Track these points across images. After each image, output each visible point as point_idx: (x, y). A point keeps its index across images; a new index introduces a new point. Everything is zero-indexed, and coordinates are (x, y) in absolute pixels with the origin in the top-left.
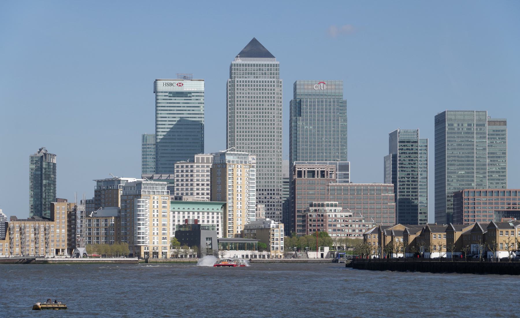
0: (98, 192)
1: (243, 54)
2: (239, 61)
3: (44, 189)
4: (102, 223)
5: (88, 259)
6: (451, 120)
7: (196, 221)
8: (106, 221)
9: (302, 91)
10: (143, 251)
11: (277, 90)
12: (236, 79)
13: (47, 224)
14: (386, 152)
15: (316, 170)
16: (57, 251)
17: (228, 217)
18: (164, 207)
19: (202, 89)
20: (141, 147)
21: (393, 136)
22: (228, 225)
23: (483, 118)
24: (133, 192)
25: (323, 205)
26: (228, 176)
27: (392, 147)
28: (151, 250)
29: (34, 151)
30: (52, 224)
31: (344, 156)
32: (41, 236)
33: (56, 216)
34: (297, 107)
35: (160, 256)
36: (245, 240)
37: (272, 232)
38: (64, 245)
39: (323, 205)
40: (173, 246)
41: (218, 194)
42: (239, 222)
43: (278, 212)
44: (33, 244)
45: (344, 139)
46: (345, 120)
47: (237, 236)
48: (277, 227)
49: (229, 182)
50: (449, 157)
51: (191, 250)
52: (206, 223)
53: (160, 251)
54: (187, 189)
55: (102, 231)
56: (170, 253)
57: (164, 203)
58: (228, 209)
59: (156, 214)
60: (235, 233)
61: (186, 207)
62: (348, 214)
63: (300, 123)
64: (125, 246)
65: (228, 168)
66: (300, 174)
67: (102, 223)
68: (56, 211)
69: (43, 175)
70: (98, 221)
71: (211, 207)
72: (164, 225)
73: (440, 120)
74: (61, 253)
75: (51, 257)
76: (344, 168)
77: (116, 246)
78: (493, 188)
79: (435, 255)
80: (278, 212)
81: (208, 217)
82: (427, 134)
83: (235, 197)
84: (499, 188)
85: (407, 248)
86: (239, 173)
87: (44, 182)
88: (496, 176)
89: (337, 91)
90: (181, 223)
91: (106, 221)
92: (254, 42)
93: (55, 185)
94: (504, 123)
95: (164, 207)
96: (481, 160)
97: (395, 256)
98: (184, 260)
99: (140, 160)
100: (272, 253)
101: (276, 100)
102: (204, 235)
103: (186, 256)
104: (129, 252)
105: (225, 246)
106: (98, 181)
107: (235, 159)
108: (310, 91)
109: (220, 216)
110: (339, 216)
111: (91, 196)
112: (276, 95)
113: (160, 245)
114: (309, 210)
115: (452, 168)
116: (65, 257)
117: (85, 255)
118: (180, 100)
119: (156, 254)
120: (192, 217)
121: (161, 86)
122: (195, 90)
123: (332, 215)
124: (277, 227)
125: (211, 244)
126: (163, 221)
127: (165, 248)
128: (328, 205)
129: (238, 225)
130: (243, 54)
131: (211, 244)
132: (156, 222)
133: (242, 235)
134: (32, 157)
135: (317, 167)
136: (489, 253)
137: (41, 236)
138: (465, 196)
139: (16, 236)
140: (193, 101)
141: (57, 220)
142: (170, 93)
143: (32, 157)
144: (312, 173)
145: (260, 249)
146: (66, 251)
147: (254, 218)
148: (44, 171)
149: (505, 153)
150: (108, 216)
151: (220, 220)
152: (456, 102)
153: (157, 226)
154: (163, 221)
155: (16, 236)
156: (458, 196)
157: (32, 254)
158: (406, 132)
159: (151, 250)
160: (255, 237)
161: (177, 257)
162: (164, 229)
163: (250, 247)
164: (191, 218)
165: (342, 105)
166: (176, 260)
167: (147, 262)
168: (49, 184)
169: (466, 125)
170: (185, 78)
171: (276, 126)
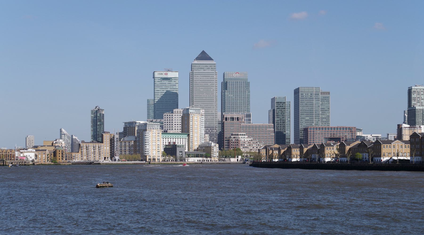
0: (124, 128)
1: (198, 59)
2: (196, 62)
3: (98, 127)
5: (120, 162)
6: (302, 91)
7: (174, 143)
8: (129, 143)
9: (227, 77)
10: (148, 158)
11: (215, 76)
12: (194, 71)
13: (100, 144)
14: (270, 108)
16: (105, 158)
17: (190, 141)
18: (158, 136)
19: (177, 76)
21: (273, 100)
25: (238, 135)
26: (190, 120)
27: (273, 105)
28: (152, 158)
29: (93, 108)
30: (102, 144)
32: (97, 150)
33: (104, 140)
34: (225, 86)
35: (156, 160)
36: (199, 153)
38: (108, 155)
39: (238, 135)
40: (163, 155)
41: (185, 129)
42: (196, 143)
43: (215, 138)
46: (249, 92)
47: (195, 150)
48: (215, 146)
49: (191, 123)
50: (301, 110)
51: (172, 158)
52: (179, 144)
53: (156, 158)
54: (170, 127)
55: (127, 148)
56: (161, 159)
57: (158, 134)
59: (154, 139)
60: (194, 149)
61: (169, 136)
63: (226, 93)
64: (139, 156)
65: (191, 116)
68: (104, 138)
69: (97, 120)
70: (125, 143)
73: (297, 92)
74: (107, 159)
75: (102, 161)
76: (249, 116)
77: (134, 156)
79: (294, 160)
80: (215, 138)
81: (180, 141)
82: (290, 99)
83: (194, 131)
84: (326, 126)
85: (280, 156)
86: (196, 119)
87: (98, 123)
88: (324, 120)
89: (245, 77)
90: (167, 144)
91: (129, 143)
92: (203, 52)
95: (158, 136)
97: (274, 160)
98: (168, 162)
100: (213, 159)
101: (214, 82)
102: (178, 150)
103: (169, 160)
106: (125, 123)
108: (231, 77)
109: (186, 140)
110: (246, 140)
111: (122, 130)
112: (214, 79)
113: (156, 155)
114: (231, 137)
115: (302, 116)
116: (109, 161)
117: (119, 160)
119: (154, 159)
120: (172, 141)
121: (156, 75)
123: (243, 139)
124: (215, 146)
125: (182, 154)
127: (159, 156)
128: (240, 135)
129: (196, 145)
130: (198, 59)
131: (182, 154)
132: (154, 144)
133: (197, 150)
134: (92, 111)
135: (235, 116)
137: (97, 150)
138: (309, 130)
139: (84, 151)
140: (173, 82)
142: (161, 78)
143: (92, 111)
144: (233, 119)
145: (206, 157)
146: (109, 158)
149: (329, 109)
150: (130, 140)
151: (186, 142)
152: (304, 84)
153: (155, 146)
155: (84, 151)
156: (306, 130)
157: (92, 160)
159: (152, 158)
160: (204, 151)
161: (165, 161)
162: (158, 147)
163: (202, 156)
164: (172, 141)
165: (247, 84)
166: (164, 162)
167: (150, 163)
168: (101, 124)
169: (309, 94)
170: (169, 71)
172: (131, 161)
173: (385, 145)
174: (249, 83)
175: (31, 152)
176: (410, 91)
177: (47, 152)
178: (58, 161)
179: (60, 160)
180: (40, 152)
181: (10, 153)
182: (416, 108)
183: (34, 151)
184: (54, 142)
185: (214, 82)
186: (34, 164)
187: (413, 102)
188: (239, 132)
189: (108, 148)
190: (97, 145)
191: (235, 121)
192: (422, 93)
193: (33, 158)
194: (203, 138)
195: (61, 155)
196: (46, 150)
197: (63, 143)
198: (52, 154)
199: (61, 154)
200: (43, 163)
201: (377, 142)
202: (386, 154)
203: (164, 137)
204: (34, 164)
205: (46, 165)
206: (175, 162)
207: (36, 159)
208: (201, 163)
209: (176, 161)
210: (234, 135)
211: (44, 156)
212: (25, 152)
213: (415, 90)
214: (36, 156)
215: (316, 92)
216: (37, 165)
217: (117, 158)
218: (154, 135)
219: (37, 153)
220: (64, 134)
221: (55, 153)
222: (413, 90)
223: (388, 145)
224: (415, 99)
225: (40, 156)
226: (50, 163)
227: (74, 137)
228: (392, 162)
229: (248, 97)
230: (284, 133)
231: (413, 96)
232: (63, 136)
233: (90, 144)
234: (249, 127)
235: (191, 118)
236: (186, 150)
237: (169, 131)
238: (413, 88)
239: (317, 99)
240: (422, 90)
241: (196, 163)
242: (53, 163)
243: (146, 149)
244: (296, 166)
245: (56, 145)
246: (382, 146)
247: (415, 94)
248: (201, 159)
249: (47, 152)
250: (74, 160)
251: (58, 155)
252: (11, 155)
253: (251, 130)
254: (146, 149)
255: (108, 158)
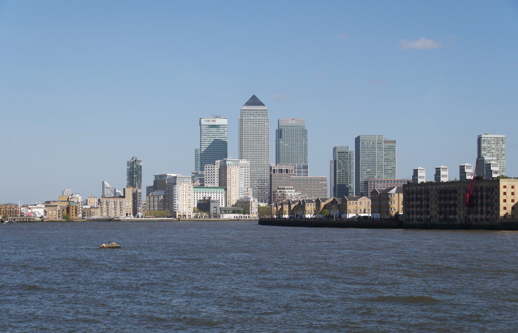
0: (155, 182)
1: (247, 104)
2: (246, 108)
3: (134, 180)
4: (156, 199)
5: (143, 219)
6: (363, 140)
7: (210, 198)
8: (158, 198)
9: (282, 124)
10: (177, 214)
11: (266, 124)
13: (121, 199)
14: (332, 159)
15: (283, 169)
16: (127, 214)
17: (228, 195)
18: (189, 190)
19: (226, 123)
20: (194, 156)
21: (335, 149)
22: (228, 200)
23: (381, 139)
24: (173, 182)
25: (284, 189)
26: (228, 173)
27: (334, 156)
28: (182, 214)
29: (129, 159)
30: (124, 200)
31: (306, 162)
32: (118, 206)
33: (126, 195)
34: (279, 133)
35: (187, 217)
36: (236, 208)
37: (251, 204)
38: (131, 211)
39: (284, 189)
40: (194, 211)
41: (223, 184)
42: (234, 198)
43: (267, 193)
44: (113, 211)
45: (306, 151)
46: (306, 141)
47: (233, 206)
48: (254, 201)
49: (228, 176)
50: (362, 161)
51: (205, 214)
52: (215, 199)
53: (187, 214)
54: (211, 180)
55: (156, 203)
56: (193, 215)
57: (189, 187)
58: (228, 191)
59: (185, 194)
60: (232, 204)
61: (207, 190)
62: (298, 194)
63: (281, 142)
64: (167, 212)
65: (228, 168)
66: (274, 170)
67: (156, 199)
68: (126, 192)
69: (134, 173)
70: (154, 198)
71: (218, 190)
72: (189, 200)
73: (357, 140)
74: (129, 215)
75: (123, 217)
76: (306, 167)
77: (162, 212)
78: (388, 178)
79: (308, 216)
80: (267, 193)
81: (216, 196)
82: (352, 148)
83: (232, 184)
84: (392, 178)
85: (291, 212)
86: (234, 171)
87: (135, 176)
88: (390, 172)
89: (302, 124)
90: (201, 199)
91: (158, 198)
92: (254, 97)
93: (141, 177)
94: (395, 142)
95: (189, 190)
96: (380, 163)
97: (284, 216)
98: (201, 219)
99: (194, 163)
100: (251, 215)
101: (265, 129)
102: (212, 205)
103: (202, 217)
104: (169, 215)
105: (226, 211)
106: (156, 176)
107: (232, 163)
108: (287, 124)
109: (223, 195)
110: (293, 195)
111: (152, 184)
112: (265, 127)
113: (187, 211)
114: (276, 192)
115: (363, 167)
116: (131, 217)
118: (214, 130)
119: (185, 216)
120: (207, 195)
121: (203, 122)
122: (222, 124)
123: (289, 194)
124: (254, 201)
125: (216, 210)
126: (189, 197)
127: (190, 213)
128: (287, 189)
129: (234, 199)
130: (247, 104)
131: (216, 210)
132: (185, 199)
133: (235, 205)
134: (128, 162)
135: (284, 168)
136: (342, 215)
137: (118, 206)
139: (105, 206)
140: (221, 130)
141: (126, 197)
143: (128, 162)
144: (281, 171)
145: (244, 213)
146: (132, 214)
147: (243, 196)
148: (134, 170)
149: (395, 159)
150: (160, 195)
151: (223, 197)
152: (365, 131)
153: (186, 201)
154: (189, 197)
155: (105, 206)
156: (366, 183)
157: (112, 215)
158: (342, 147)
159: (182, 214)
160: (243, 206)
161: (197, 217)
162: (189, 202)
163: (238, 212)
165: (304, 132)
166: (196, 219)
167: (179, 220)
168: (138, 177)
170: (217, 117)
171: (266, 144)
172: (157, 217)
173: (351, 202)
174: (307, 130)
175: (40, 208)
176: (479, 139)
177: (58, 208)
178: (71, 217)
179: (72, 217)
180: (50, 208)
181: (15, 209)
182: (485, 159)
183: (44, 206)
184: (70, 197)
185: (265, 129)
186: (42, 221)
187: (483, 152)
188: (288, 185)
189: (131, 204)
190: (118, 200)
191: (284, 173)
192: (493, 142)
193: (42, 214)
194: (242, 192)
195: (74, 211)
196: (57, 206)
197: (80, 198)
198: (65, 210)
199: (74, 210)
200: (54, 219)
201: (303, 201)
202: (352, 211)
203: (196, 191)
204: (42, 221)
205: (57, 221)
206: (208, 219)
207: (45, 215)
208: (238, 220)
209: (209, 217)
210: (280, 189)
211: (55, 212)
212: (33, 208)
213: (485, 139)
214: (45, 212)
215: (379, 140)
216: (46, 221)
217: (140, 214)
218: (185, 189)
219: (47, 209)
220: (107, 188)
221: (68, 209)
222: (483, 139)
223: (355, 202)
224: (485, 149)
225: (50, 212)
226: (62, 219)
227: (117, 191)
228: (358, 219)
229: (306, 146)
230: (347, 186)
231: (483, 145)
232: (106, 189)
233: (111, 200)
234: (307, 180)
235: (228, 171)
236: (224, 206)
237: (206, 185)
238: (483, 136)
239: (380, 149)
240: (493, 139)
241: (231, 220)
242: (65, 220)
243: (175, 205)
244: (360, 223)
245: (72, 200)
246: (348, 203)
247: (485, 143)
248: (238, 215)
249: (58, 208)
250: (93, 217)
251: (71, 211)
252: (16, 211)
253: (302, 184)
254: (175, 205)
255: (130, 214)
